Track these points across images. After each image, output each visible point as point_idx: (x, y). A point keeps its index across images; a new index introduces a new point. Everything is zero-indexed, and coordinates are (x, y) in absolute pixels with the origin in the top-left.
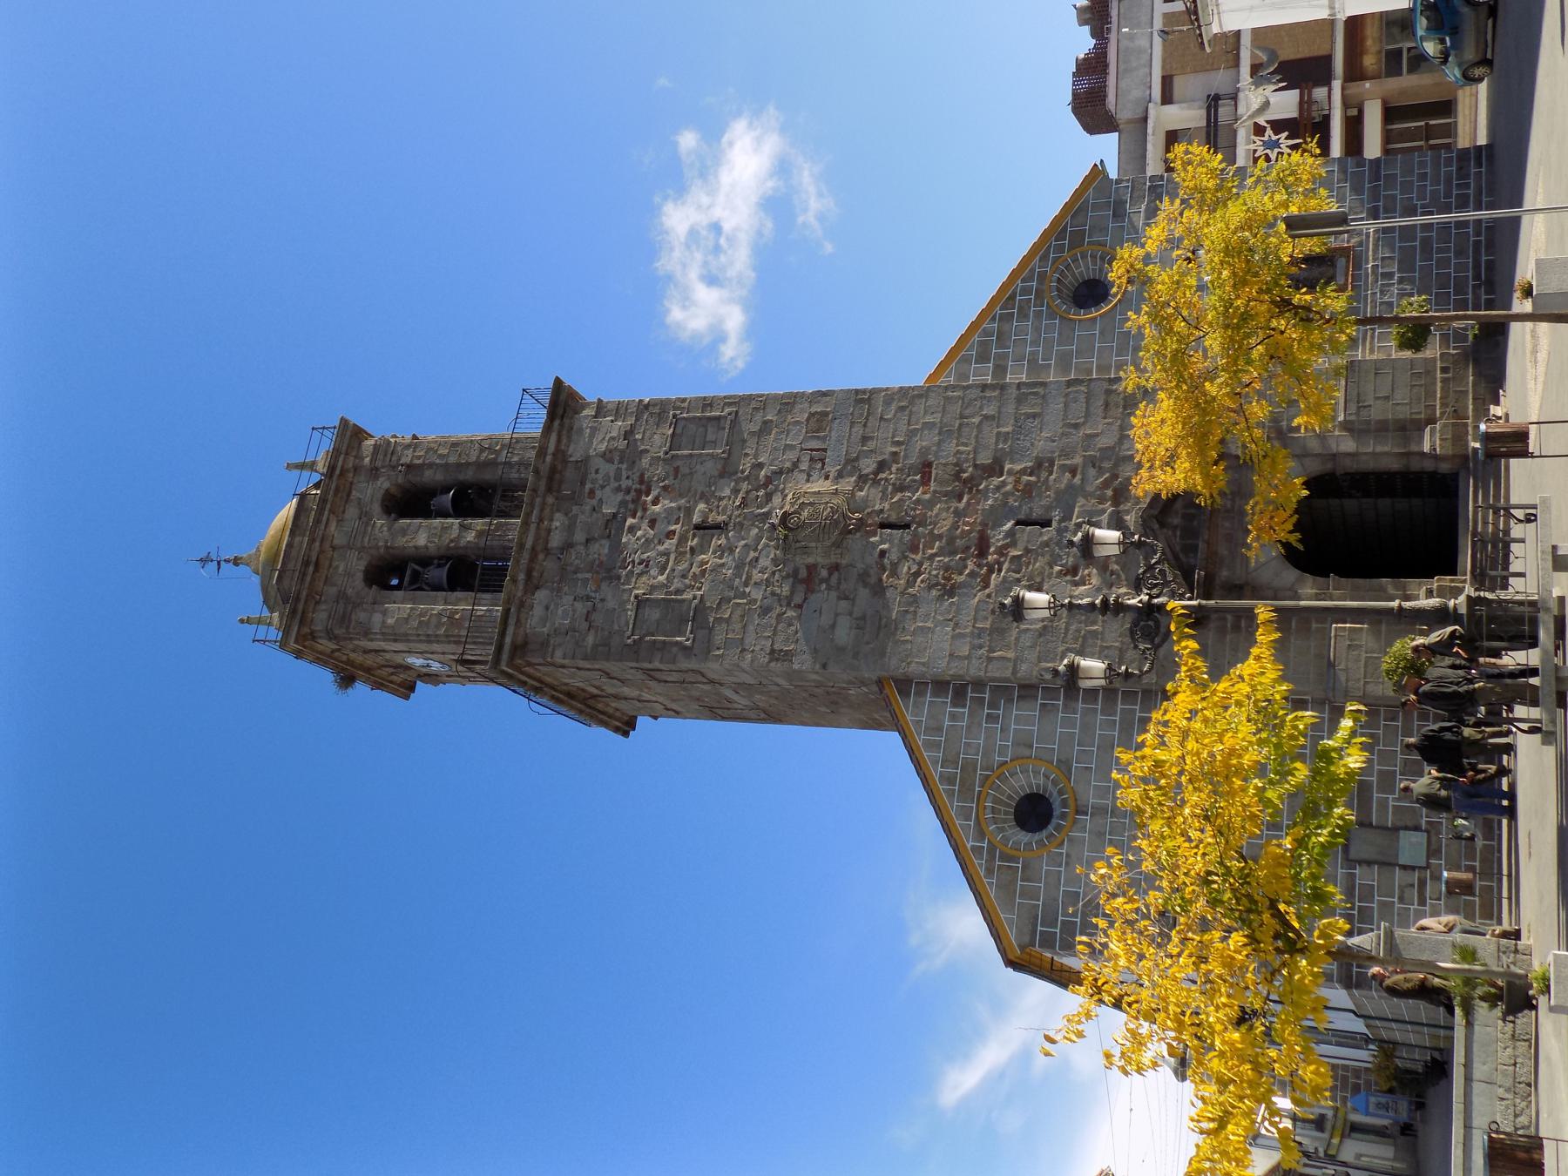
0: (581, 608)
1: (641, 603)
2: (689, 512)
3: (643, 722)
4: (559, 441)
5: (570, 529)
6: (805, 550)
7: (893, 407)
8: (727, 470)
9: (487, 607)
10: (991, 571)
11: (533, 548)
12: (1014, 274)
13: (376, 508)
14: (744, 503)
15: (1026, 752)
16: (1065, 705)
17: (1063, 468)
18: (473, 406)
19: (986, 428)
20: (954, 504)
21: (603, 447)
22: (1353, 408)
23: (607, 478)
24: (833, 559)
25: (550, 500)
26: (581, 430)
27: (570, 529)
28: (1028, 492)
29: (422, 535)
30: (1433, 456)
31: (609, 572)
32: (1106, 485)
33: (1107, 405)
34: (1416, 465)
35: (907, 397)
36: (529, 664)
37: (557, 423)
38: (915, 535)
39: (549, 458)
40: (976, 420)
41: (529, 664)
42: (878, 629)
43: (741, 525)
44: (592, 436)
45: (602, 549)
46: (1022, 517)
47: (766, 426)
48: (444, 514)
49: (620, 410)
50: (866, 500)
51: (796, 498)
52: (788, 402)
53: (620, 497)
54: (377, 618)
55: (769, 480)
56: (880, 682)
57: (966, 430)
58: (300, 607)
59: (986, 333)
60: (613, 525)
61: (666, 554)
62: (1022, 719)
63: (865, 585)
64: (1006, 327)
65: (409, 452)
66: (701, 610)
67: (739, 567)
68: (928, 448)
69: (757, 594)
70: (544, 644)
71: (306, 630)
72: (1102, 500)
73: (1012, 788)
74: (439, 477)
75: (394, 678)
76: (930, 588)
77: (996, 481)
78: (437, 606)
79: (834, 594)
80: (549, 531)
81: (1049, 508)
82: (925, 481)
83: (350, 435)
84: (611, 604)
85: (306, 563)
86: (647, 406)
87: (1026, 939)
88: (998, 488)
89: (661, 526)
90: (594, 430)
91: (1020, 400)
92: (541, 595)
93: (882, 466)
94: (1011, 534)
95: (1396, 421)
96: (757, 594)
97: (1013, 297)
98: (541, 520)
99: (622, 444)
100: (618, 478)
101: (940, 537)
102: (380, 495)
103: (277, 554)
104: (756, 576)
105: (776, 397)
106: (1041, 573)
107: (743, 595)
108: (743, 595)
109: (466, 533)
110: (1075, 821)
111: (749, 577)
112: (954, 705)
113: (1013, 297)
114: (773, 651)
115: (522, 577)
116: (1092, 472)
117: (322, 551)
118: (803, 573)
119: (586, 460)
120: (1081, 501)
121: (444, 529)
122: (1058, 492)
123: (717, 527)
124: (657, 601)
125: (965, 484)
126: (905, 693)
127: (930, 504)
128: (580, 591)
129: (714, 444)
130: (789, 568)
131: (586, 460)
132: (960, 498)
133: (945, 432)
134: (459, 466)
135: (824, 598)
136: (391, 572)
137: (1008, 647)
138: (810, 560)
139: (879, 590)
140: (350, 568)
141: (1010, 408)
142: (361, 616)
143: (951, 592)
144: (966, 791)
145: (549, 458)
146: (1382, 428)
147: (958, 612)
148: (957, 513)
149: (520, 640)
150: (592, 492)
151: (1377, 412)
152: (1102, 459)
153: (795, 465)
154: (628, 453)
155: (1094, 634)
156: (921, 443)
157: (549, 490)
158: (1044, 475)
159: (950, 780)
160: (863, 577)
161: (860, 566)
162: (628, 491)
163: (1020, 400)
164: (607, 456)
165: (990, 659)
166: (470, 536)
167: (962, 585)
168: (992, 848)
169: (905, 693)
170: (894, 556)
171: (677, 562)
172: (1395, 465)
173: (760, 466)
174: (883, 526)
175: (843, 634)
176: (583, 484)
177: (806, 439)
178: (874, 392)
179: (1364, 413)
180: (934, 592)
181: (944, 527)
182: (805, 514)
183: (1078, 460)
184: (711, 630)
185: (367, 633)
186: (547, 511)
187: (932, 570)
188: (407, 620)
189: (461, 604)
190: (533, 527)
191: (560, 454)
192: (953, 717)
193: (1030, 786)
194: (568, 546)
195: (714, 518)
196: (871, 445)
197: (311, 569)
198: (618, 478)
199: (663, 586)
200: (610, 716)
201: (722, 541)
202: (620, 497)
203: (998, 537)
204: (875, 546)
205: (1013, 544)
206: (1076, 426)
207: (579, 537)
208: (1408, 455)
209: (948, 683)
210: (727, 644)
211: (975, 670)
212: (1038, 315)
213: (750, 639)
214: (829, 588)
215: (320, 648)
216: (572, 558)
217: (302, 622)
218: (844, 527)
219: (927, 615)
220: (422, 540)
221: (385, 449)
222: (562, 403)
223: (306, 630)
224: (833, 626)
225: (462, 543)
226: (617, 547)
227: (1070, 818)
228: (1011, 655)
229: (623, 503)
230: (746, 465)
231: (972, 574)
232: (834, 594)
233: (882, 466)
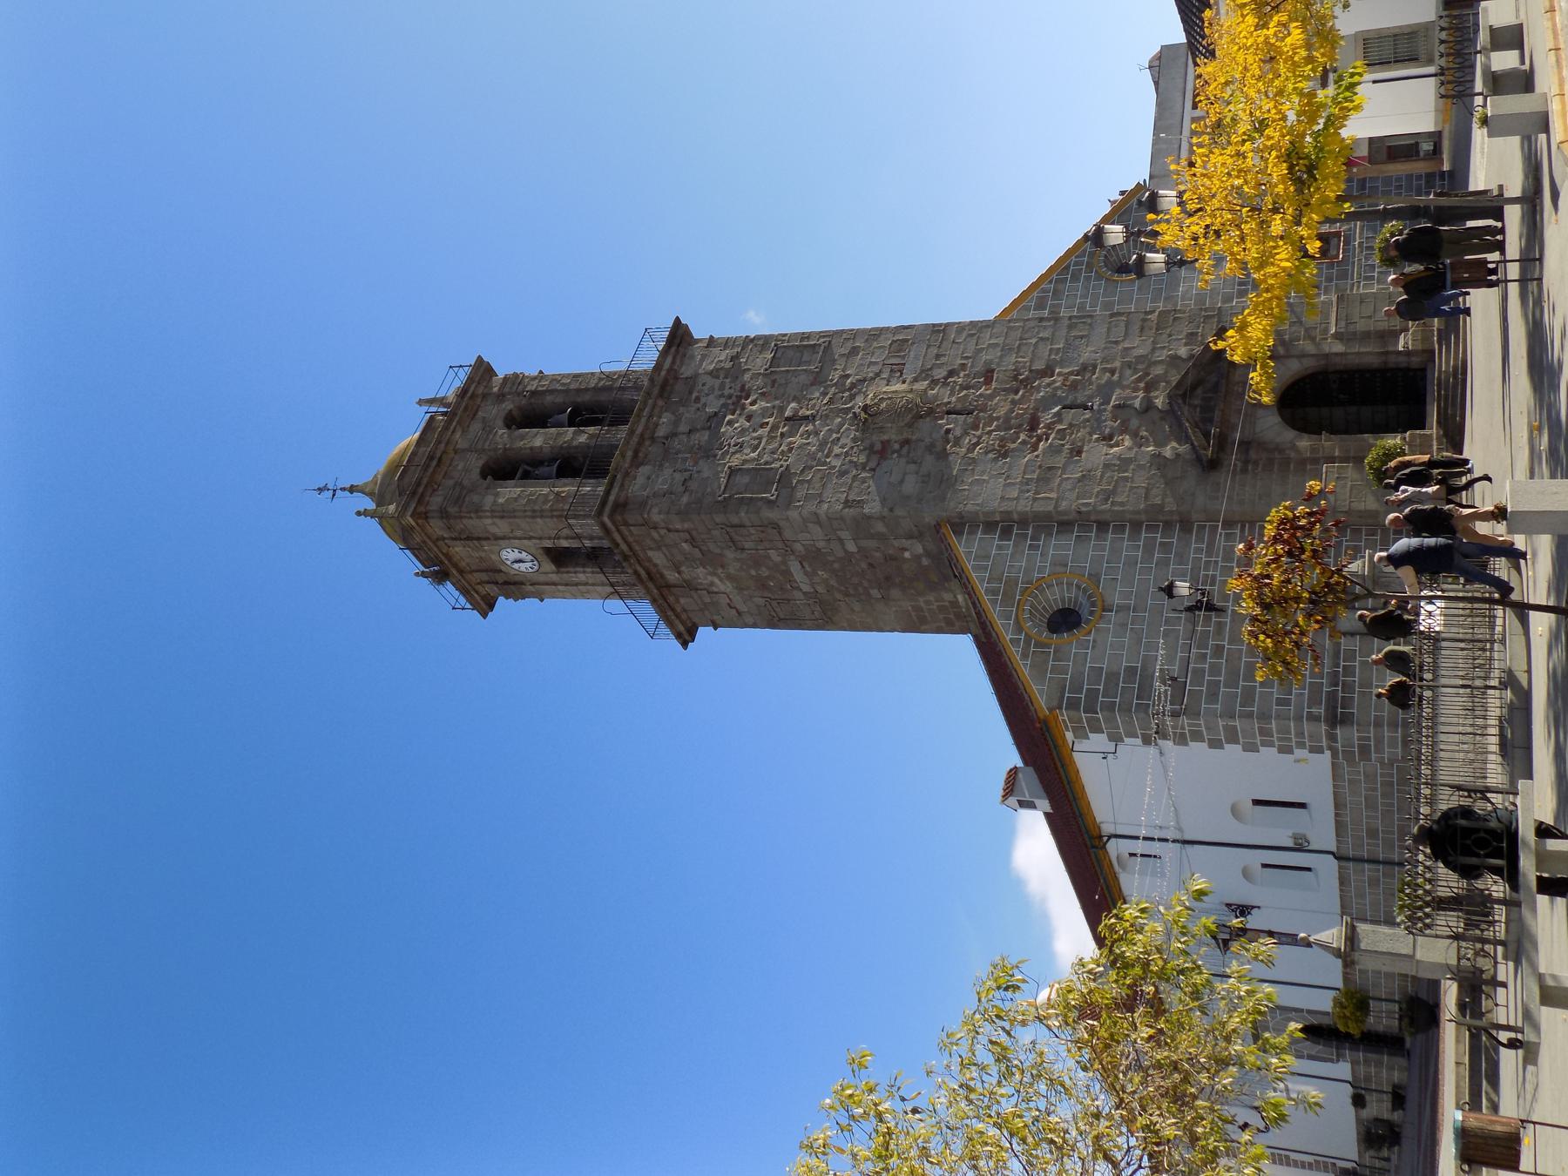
0: (679, 477)
1: (733, 471)
2: (782, 409)
3: (704, 632)
4: (673, 362)
5: (676, 423)
6: (881, 429)
7: (964, 335)
8: (818, 379)
9: (590, 488)
10: (1040, 440)
11: (642, 435)
12: (1069, 253)
13: (500, 422)
14: (831, 401)
15: (1062, 569)
16: (1097, 536)
17: (1104, 370)
18: (597, 338)
19: (1041, 345)
20: (1011, 397)
21: (712, 367)
22: (1343, 324)
23: (712, 389)
24: (905, 435)
25: (660, 403)
26: (692, 357)
27: (676, 423)
28: (1074, 386)
29: (538, 439)
30: (1408, 353)
31: (707, 453)
32: (1139, 380)
33: (1142, 329)
34: (1392, 359)
35: (977, 328)
36: (626, 524)
37: (673, 349)
38: (977, 417)
39: (663, 373)
40: (1034, 341)
41: (626, 524)
42: (944, 483)
43: (827, 416)
44: (702, 361)
45: (704, 437)
46: (1068, 402)
47: (854, 351)
48: (559, 425)
49: (727, 343)
50: (936, 397)
51: (875, 396)
52: (875, 334)
53: (722, 401)
54: (489, 499)
55: (853, 385)
56: (938, 527)
57: (1024, 348)
58: (421, 490)
59: (1044, 291)
60: (715, 420)
61: (760, 438)
62: (1058, 547)
63: (931, 453)
64: (1060, 287)
65: (535, 383)
66: (786, 474)
67: (823, 444)
68: (991, 362)
69: (837, 463)
70: (643, 504)
71: (422, 509)
72: (1136, 390)
73: (1047, 600)
74: (559, 399)
75: (479, 588)
76: (986, 453)
77: (1047, 380)
78: (542, 489)
79: (903, 460)
80: (657, 425)
81: (1090, 398)
82: (988, 381)
83: (482, 370)
84: (706, 474)
85: (431, 458)
86: (752, 340)
87: (1055, 703)
88: (1049, 385)
89: (757, 420)
90: (704, 357)
91: (1070, 327)
92: (645, 470)
93: (951, 373)
94: (1058, 414)
95: (1377, 332)
96: (837, 463)
97: (1067, 268)
98: (650, 416)
99: (728, 365)
100: (722, 386)
101: (998, 418)
102: (503, 414)
103: (398, 466)
104: (837, 450)
105: (864, 331)
106: (1083, 440)
107: (825, 463)
108: (825, 463)
109: (581, 437)
110: (1101, 617)
111: (830, 451)
112: (1001, 539)
113: (1067, 268)
114: (847, 501)
115: (630, 454)
116: (1128, 372)
117: (444, 452)
118: (878, 447)
119: (696, 376)
120: (1118, 391)
121: (559, 434)
122: (1099, 386)
123: (806, 418)
124: (748, 470)
125: (1021, 382)
126: (958, 533)
127: (991, 397)
128: (678, 466)
129: (809, 363)
130: (867, 443)
131: (696, 376)
132: (1016, 392)
133: (1006, 350)
134: (578, 391)
135: (895, 466)
136: (503, 469)
137: (1052, 490)
138: (886, 437)
139: (943, 455)
140: (469, 467)
141: (1064, 332)
142: (476, 498)
143: (1005, 456)
144: (1008, 598)
145: (663, 373)
146: (1366, 336)
147: (1010, 468)
148: (1013, 402)
149: (622, 500)
150: (698, 399)
151: (1361, 326)
152: (1137, 363)
153: (877, 375)
154: (734, 370)
155: (1126, 479)
156: (984, 357)
157: (661, 395)
158: (1088, 375)
159: (995, 592)
160: (930, 448)
161: (927, 440)
162: (730, 397)
163: (1070, 327)
164: (713, 374)
165: (1035, 499)
166: (583, 439)
167: (1014, 450)
168: (1028, 639)
169: (958, 533)
170: (958, 432)
171: (768, 443)
172: (1375, 362)
173: (848, 376)
174: (949, 413)
175: (910, 486)
176: (690, 393)
177: (888, 358)
178: (948, 325)
179: (1351, 327)
180: (991, 456)
181: (1002, 412)
182: (884, 405)
183: (1117, 364)
184: (793, 488)
185: (478, 510)
186: (656, 411)
187: (992, 440)
188: (516, 500)
189: (567, 487)
190: (643, 420)
191: (673, 374)
192: (999, 547)
193: (1063, 600)
194: (674, 435)
195: (804, 412)
196: (943, 360)
197: (434, 463)
198: (722, 386)
199: (754, 459)
200: (678, 616)
201: (810, 427)
202: (722, 401)
203: (1047, 418)
204: (941, 426)
205: (1060, 421)
206: (1116, 343)
207: (683, 428)
208: (1387, 353)
209: (997, 523)
210: (807, 498)
211: (1024, 506)
212: (1088, 279)
213: (828, 494)
214: (900, 456)
215: (430, 531)
216: (676, 444)
217: (420, 502)
218: (919, 413)
219: (983, 473)
220: (538, 442)
221: (515, 380)
222: (679, 336)
223: (422, 509)
224: (902, 481)
225: (575, 443)
226: (716, 434)
227: (1097, 615)
228: (1053, 495)
229: (724, 405)
230: (835, 376)
231: (1024, 442)
232: (903, 460)
233: (951, 373)
